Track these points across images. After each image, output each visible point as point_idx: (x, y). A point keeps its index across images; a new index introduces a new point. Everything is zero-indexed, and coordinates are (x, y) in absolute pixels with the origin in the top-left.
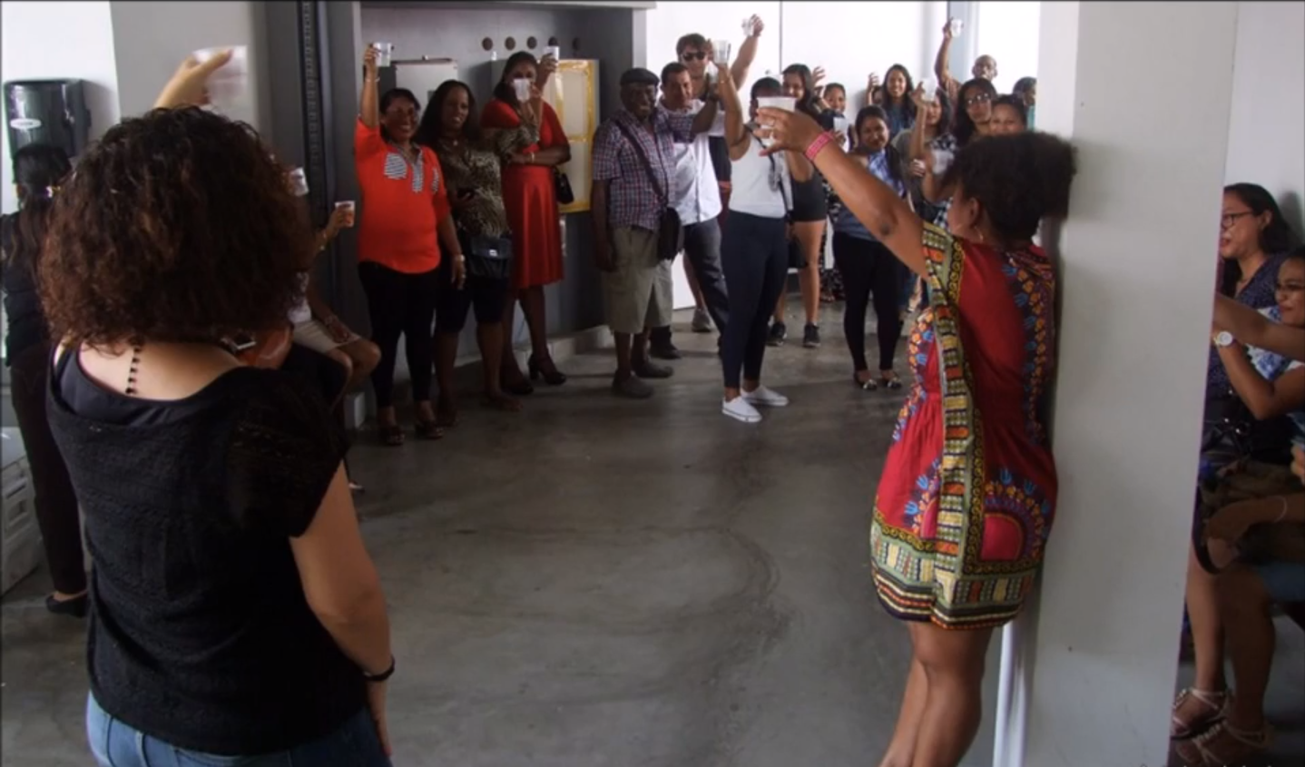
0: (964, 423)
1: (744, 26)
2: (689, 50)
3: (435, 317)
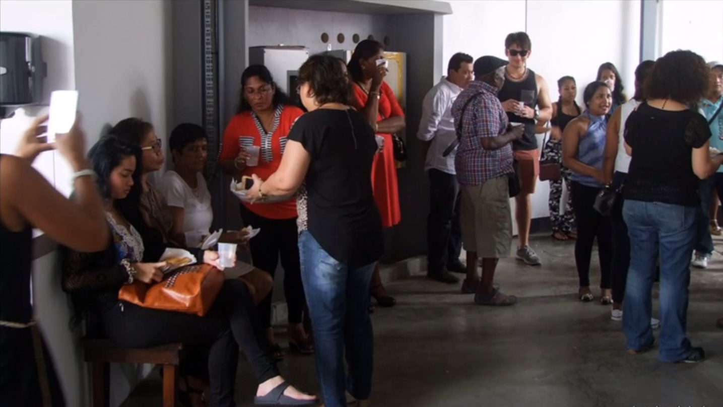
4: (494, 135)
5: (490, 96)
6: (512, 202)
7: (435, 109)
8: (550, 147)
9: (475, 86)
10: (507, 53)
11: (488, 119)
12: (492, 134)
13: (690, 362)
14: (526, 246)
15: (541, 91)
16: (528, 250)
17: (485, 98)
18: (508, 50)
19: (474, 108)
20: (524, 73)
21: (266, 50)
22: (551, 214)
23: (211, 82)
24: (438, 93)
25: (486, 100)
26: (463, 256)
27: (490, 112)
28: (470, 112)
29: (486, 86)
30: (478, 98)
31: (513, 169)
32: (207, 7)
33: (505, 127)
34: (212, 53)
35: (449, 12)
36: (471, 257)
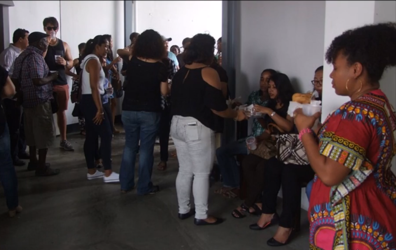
0: (360, 179)
1: (312, 81)
2: (49, 25)
3: (184, 80)
4: (41, 77)
5: (38, 55)
6: (55, 115)
7: (6, 63)
8: (77, 83)
9: (29, 49)
10: (45, 29)
11: (37, 68)
12: (40, 76)
13: (152, 193)
14: (65, 140)
15: (66, 51)
16: (66, 142)
17: (35, 56)
18: (46, 27)
19: (28, 62)
20: (56, 41)
22: (79, 121)
24: (7, 53)
25: (36, 57)
26: (27, 149)
27: (38, 64)
28: (25, 64)
29: (36, 49)
30: (31, 56)
31: (53, 97)
33: (47, 73)
36: (32, 150)
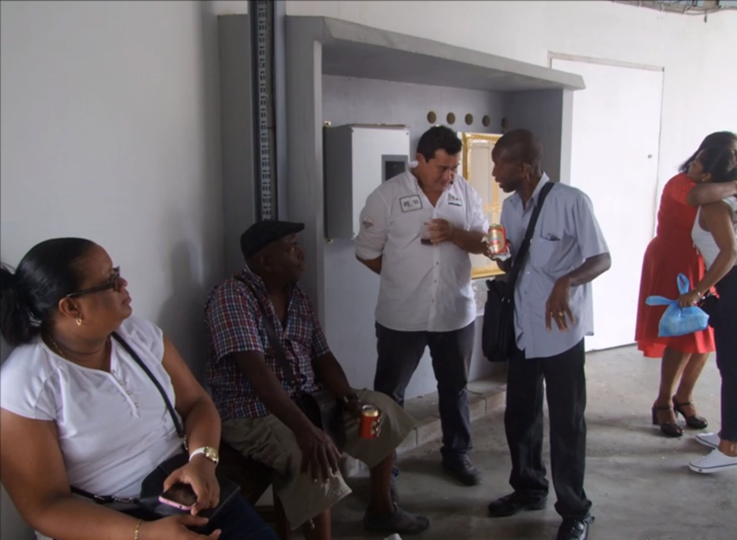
21: (353, 129)
23: (267, 168)
32: (261, 65)
34: (269, 128)
35: (581, 86)
